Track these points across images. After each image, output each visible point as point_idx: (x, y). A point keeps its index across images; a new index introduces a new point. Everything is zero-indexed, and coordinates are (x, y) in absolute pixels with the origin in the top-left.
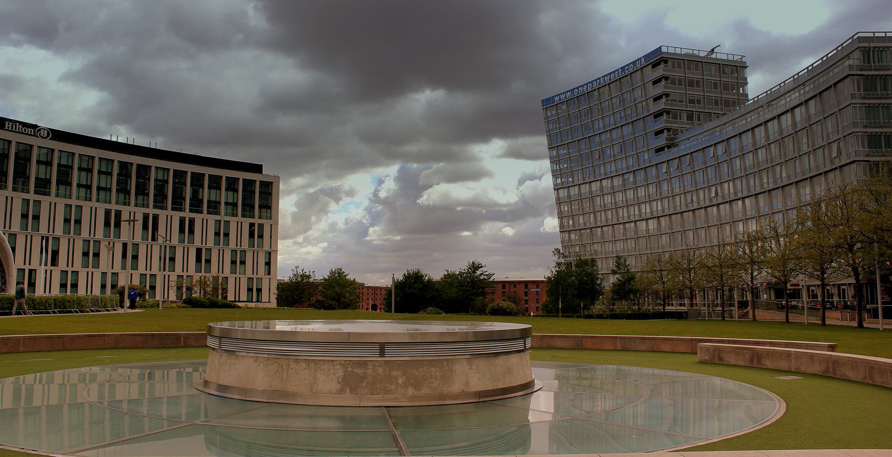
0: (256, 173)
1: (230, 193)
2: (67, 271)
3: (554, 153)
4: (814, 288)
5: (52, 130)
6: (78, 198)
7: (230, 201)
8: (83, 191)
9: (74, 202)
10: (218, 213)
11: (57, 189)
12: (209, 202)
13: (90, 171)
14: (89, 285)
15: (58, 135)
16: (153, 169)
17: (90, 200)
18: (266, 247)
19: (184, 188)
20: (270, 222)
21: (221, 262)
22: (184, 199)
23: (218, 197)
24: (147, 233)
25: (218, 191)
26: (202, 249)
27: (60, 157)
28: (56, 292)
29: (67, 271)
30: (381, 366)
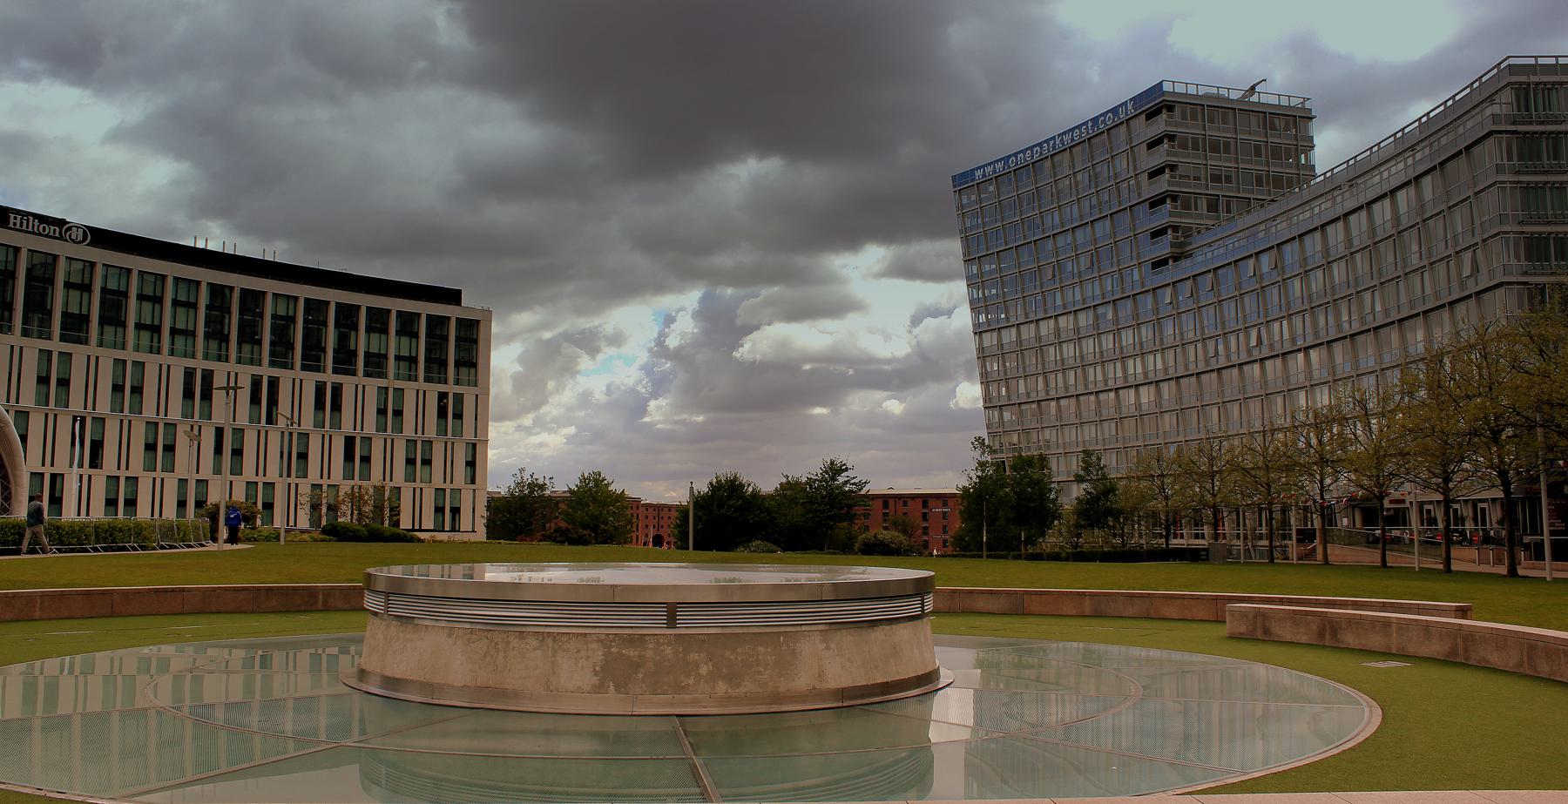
0: (451, 304)
1: (405, 340)
2: (118, 478)
3: (975, 269)
4: (1431, 507)
5: (91, 229)
6: (137, 348)
7: (405, 353)
8: (145, 335)
9: (130, 355)
10: (383, 375)
11: (100, 332)
12: (367, 355)
13: (158, 300)
14: (157, 502)
15: (102, 238)
16: (269, 298)
17: (159, 352)
18: (468, 435)
19: (324, 331)
20: (474, 390)
21: (388, 460)
22: (324, 350)
23: (383, 347)
24: (258, 410)
25: (383, 337)
26: (354, 437)
27: (106, 277)
28: (98, 513)
29: (118, 478)
30: (669, 644)
